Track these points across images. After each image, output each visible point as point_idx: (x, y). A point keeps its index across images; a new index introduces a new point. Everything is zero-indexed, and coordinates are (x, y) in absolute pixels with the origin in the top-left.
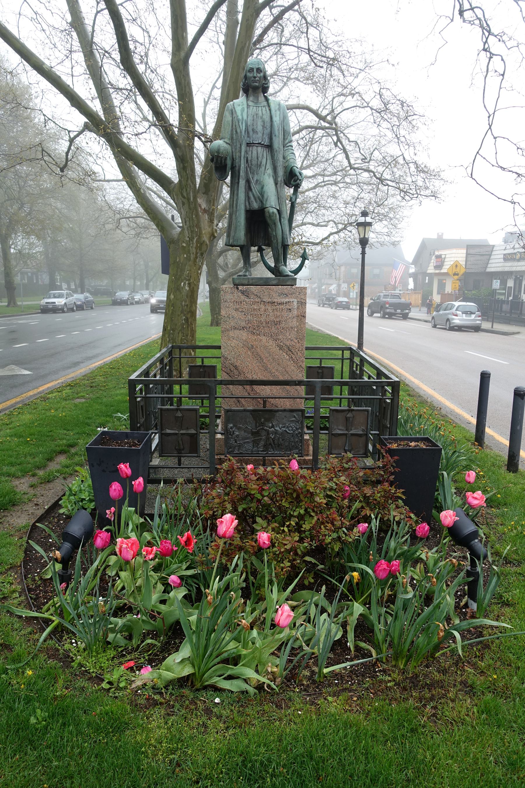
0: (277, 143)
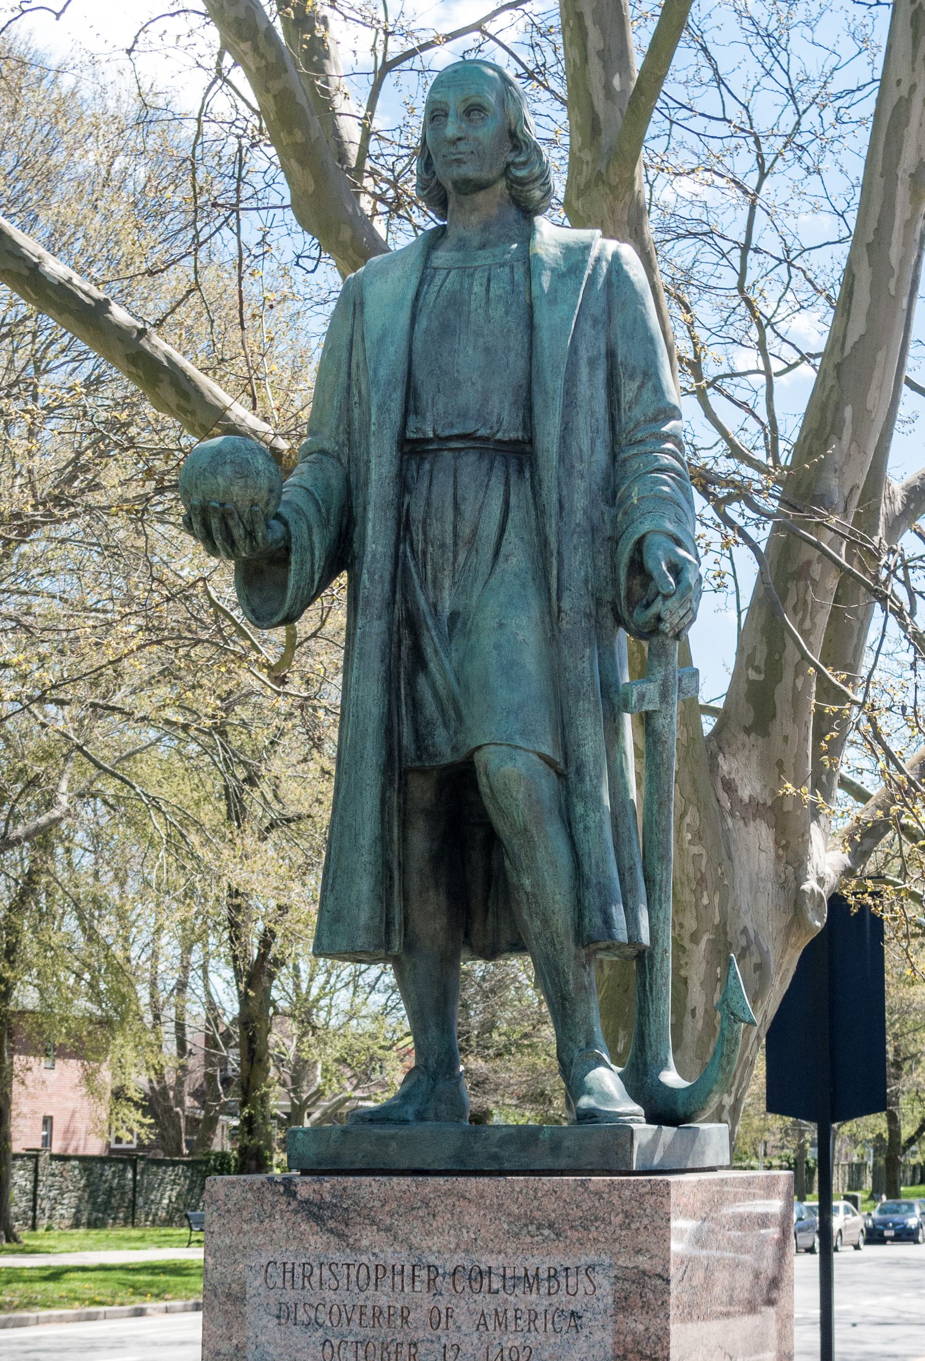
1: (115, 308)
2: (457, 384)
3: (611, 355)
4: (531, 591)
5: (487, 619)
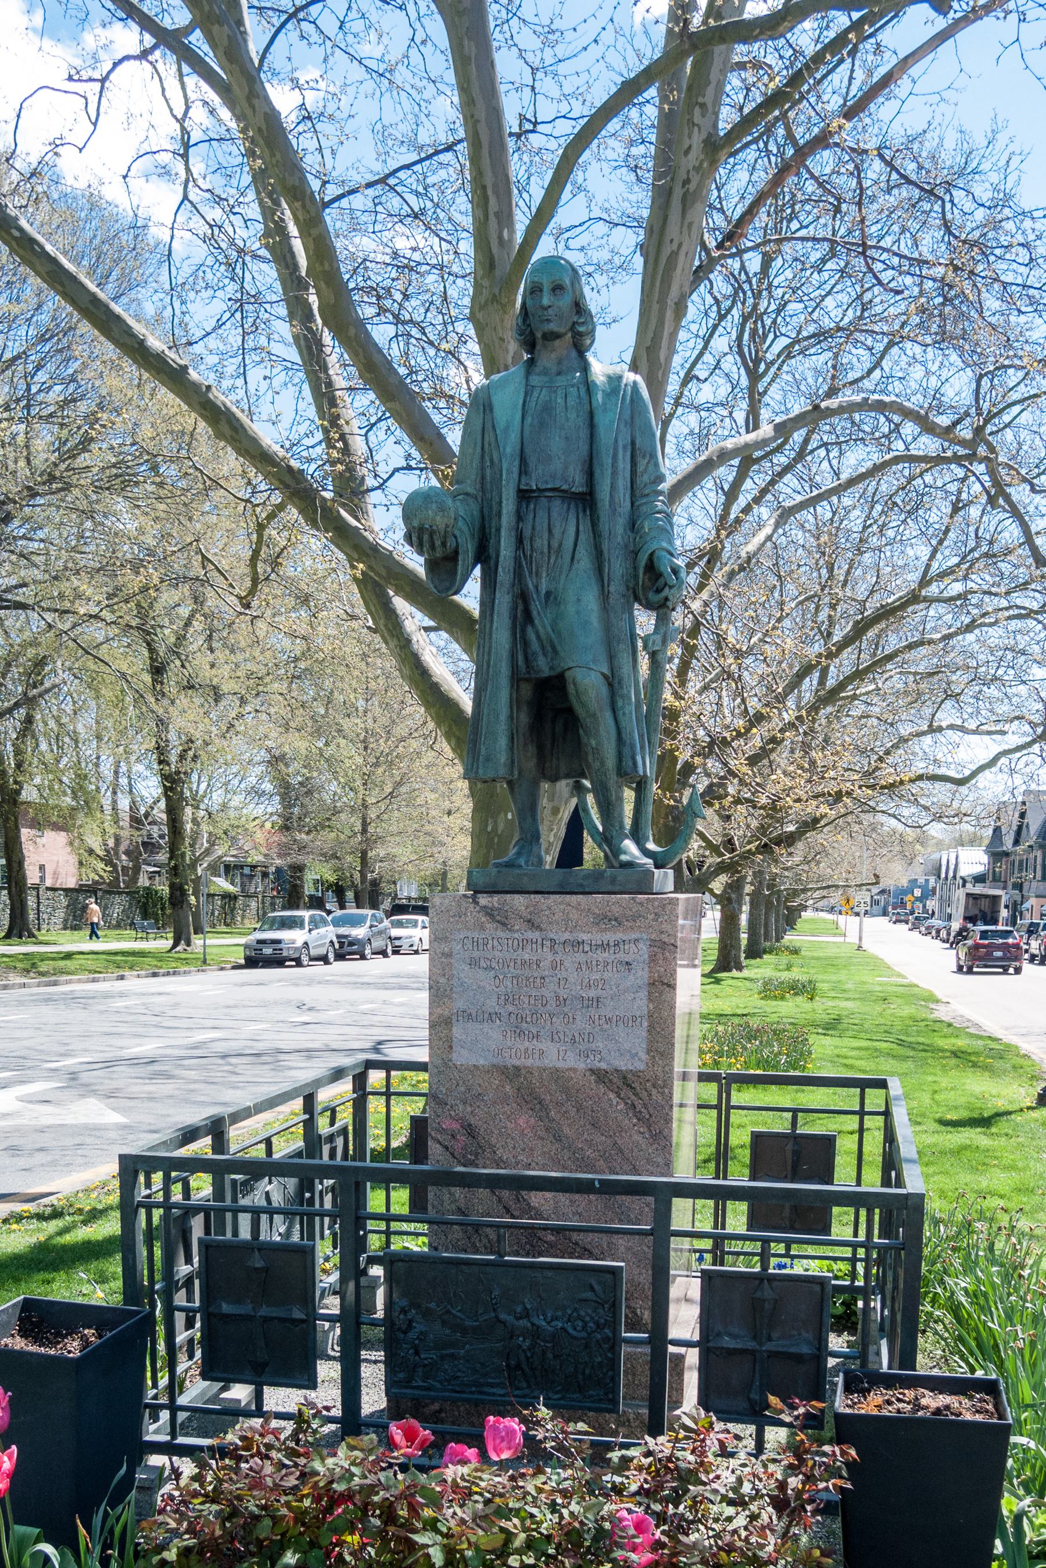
0: (613, 491)
1: (191, 371)
2: (550, 458)
3: (633, 443)
4: (593, 580)
5: (570, 596)
